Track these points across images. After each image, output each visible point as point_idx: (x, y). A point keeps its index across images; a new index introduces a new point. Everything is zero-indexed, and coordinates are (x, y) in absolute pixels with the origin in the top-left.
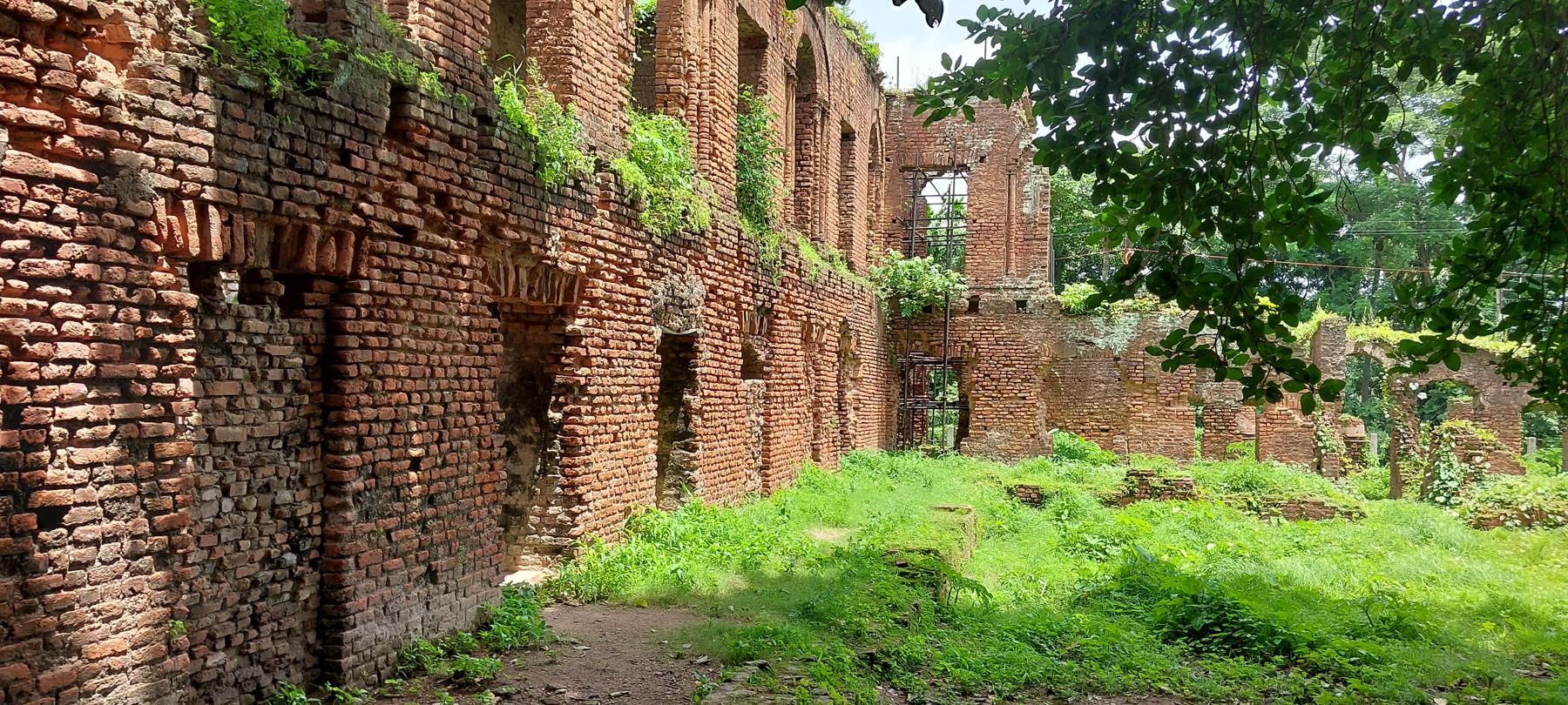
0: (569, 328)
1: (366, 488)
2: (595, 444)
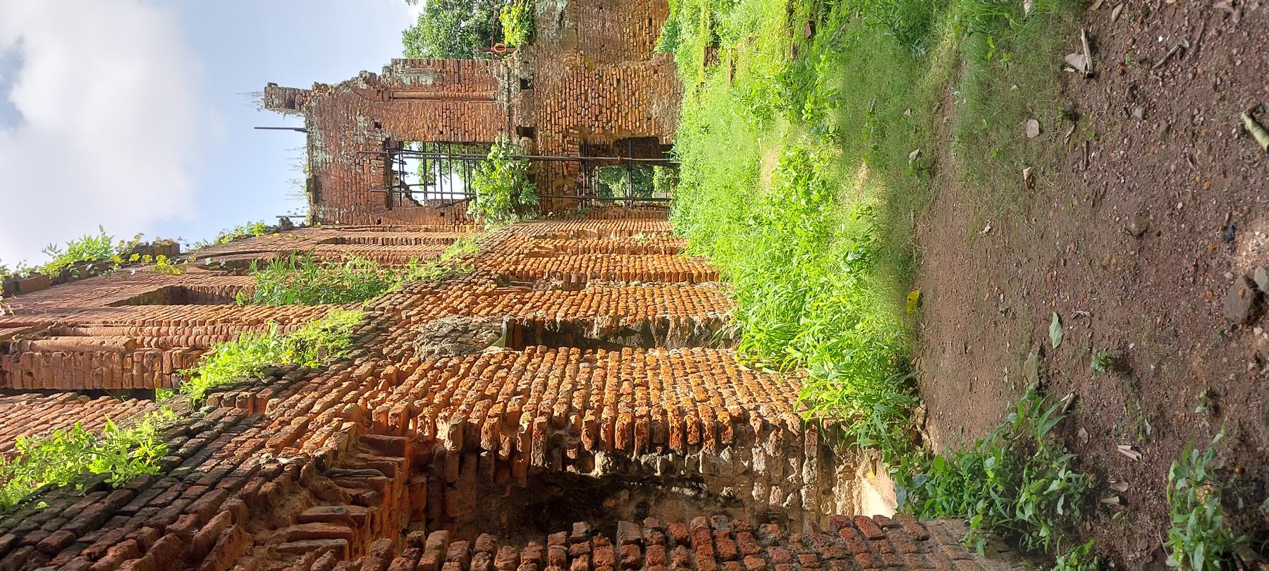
0: (448, 445)
2: (649, 404)
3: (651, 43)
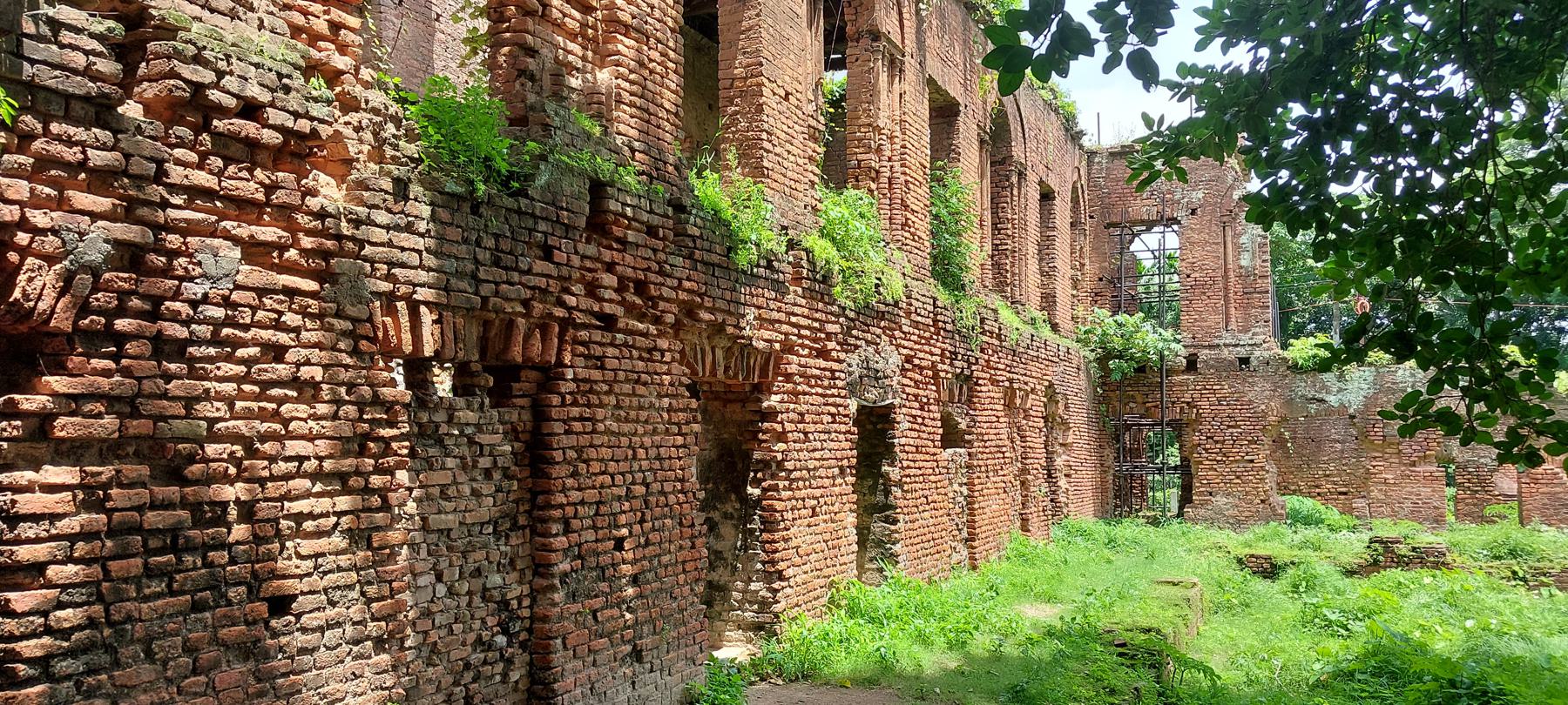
0: (765, 404)
1: (572, 570)
2: (794, 519)
3: (1319, 494)
